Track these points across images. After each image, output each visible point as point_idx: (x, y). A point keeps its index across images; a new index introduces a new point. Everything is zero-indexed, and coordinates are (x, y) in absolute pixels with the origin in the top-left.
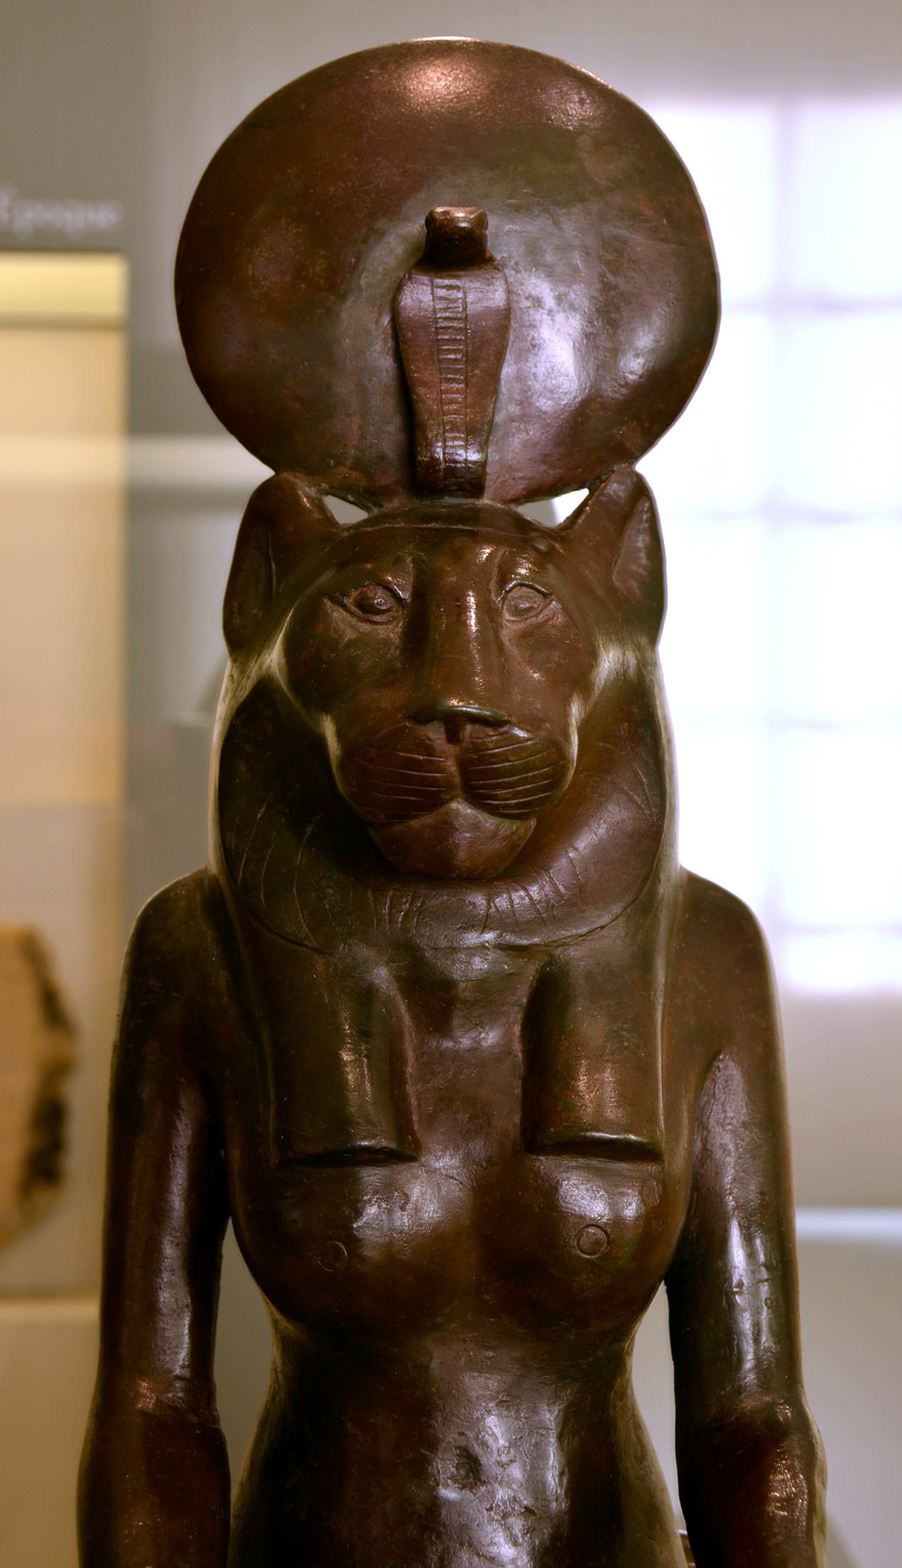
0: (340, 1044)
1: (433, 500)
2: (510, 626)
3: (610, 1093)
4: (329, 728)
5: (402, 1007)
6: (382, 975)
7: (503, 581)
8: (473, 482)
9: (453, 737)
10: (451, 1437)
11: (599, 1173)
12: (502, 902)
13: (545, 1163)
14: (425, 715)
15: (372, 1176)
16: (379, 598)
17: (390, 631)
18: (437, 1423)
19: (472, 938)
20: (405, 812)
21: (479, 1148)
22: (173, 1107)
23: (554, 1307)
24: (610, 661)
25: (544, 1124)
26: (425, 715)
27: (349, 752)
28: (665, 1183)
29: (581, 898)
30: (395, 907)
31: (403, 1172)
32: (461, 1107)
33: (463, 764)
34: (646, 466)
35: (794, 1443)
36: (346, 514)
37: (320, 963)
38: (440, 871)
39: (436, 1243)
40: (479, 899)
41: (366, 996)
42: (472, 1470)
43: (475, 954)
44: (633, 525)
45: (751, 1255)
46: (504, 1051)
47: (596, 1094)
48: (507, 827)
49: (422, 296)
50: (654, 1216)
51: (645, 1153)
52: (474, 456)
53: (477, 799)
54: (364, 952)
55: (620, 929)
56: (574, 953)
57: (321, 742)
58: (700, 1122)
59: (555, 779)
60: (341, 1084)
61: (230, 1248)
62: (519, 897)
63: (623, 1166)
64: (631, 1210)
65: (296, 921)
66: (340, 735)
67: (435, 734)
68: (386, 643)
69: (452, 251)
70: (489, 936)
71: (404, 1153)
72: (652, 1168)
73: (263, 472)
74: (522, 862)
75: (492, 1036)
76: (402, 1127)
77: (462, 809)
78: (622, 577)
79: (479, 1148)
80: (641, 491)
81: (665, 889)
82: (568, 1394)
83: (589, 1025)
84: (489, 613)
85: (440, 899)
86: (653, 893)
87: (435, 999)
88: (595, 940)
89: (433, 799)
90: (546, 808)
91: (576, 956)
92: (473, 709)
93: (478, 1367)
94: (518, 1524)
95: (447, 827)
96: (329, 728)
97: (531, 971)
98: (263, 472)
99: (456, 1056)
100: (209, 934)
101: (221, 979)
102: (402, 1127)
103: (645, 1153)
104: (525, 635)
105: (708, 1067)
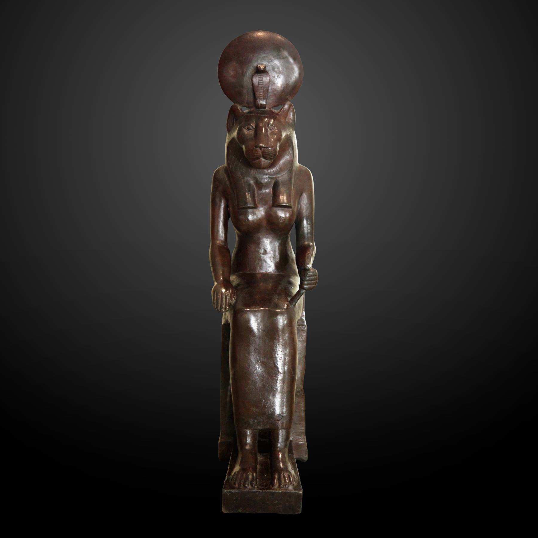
0: (246, 192)
2: (269, 131)
3: (285, 199)
4: (244, 147)
5: (255, 187)
6: (252, 182)
7: (268, 125)
8: (264, 107)
9: (261, 149)
10: (262, 247)
11: (283, 210)
12: (269, 171)
13: (275, 209)
14: (257, 147)
15: (250, 210)
16: (250, 127)
17: (252, 132)
18: (261, 245)
19: (265, 176)
20: (255, 160)
21: (266, 207)
22: (221, 201)
24: (284, 135)
25: (276, 203)
26: (257, 147)
27: (246, 151)
28: (293, 211)
29: (281, 170)
30: (253, 172)
31: (255, 210)
32: (264, 201)
33: (262, 153)
36: (246, 111)
37: (243, 181)
38: (259, 167)
39: (260, 221)
40: (266, 171)
41: (250, 185)
42: (265, 252)
43: (265, 179)
46: (270, 193)
47: (283, 199)
48: (269, 161)
49: (256, 80)
50: (291, 216)
51: (289, 207)
52: (264, 103)
53: (264, 158)
54: (249, 179)
55: (287, 175)
56: (280, 178)
57: (242, 149)
58: (299, 203)
59: (275, 155)
60: (246, 198)
62: (272, 170)
63: (286, 209)
64: (288, 215)
65: (239, 174)
66: (246, 148)
67: (258, 149)
68: (251, 134)
69: (259, 71)
70: (267, 176)
71: (255, 207)
72: (291, 209)
73: (233, 104)
74: (272, 166)
75: (268, 191)
76: (255, 203)
77: (262, 159)
79: (266, 207)
81: (294, 169)
82: (280, 241)
83: (282, 189)
84: (266, 130)
85: (260, 170)
86: (292, 169)
87: (260, 185)
88: (283, 177)
89: (258, 158)
91: (280, 179)
92: (263, 146)
93: (266, 238)
94: (272, 259)
95: (260, 162)
96: (244, 147)
97: (273, 181)
99: (263, 193)
100: (226, 176)
101: (228, 183)
102: (255, 203)
103: (289, 207)
104: (271, 133)
105: (301, 195)
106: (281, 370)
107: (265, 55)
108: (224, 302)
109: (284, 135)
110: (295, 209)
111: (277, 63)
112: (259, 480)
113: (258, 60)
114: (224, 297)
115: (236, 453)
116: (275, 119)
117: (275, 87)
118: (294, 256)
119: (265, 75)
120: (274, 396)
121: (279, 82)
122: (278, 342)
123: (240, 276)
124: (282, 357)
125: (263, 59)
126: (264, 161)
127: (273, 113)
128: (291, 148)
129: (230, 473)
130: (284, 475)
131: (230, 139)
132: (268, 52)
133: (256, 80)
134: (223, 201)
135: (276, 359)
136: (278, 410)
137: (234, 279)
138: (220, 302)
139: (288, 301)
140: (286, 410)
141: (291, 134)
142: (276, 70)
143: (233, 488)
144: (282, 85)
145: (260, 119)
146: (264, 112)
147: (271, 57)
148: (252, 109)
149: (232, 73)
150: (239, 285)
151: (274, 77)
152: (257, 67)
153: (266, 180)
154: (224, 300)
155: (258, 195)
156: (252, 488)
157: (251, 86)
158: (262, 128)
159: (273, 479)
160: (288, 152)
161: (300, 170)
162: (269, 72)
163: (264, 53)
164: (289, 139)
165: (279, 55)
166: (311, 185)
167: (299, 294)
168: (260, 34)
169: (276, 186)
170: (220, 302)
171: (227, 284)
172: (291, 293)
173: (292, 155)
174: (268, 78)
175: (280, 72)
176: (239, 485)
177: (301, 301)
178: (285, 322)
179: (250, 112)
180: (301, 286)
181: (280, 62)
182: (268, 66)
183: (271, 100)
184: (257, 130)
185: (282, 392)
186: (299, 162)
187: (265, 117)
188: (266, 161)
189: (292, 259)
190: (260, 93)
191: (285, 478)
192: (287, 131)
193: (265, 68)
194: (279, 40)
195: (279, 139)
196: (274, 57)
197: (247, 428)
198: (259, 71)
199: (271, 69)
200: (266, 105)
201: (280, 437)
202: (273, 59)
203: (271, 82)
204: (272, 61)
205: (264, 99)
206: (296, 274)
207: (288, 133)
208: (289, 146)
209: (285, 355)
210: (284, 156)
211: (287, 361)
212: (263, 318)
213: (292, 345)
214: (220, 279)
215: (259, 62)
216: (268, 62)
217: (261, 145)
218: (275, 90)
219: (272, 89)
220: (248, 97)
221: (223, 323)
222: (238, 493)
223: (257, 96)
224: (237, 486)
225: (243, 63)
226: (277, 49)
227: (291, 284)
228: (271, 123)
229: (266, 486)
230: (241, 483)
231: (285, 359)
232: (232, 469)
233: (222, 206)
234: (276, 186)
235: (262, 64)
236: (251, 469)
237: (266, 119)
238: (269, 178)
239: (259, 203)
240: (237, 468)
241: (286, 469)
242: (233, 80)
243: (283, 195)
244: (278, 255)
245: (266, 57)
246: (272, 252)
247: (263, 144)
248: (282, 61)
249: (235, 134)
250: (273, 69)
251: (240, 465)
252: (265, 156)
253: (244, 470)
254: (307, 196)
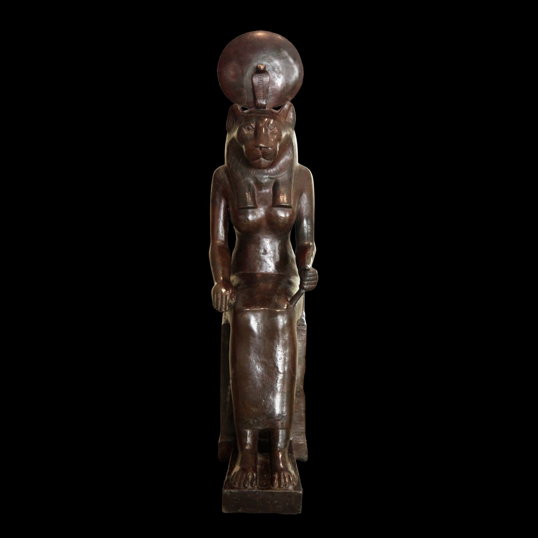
0: (246, 192)
2: (269, 131)
3: (285, 199)
4: (244, 147)
5: (255, 187)
6: (252, 182)
7: (268, 125)
8: (264, 107)
9: (261, 149)
10: (262, 247)
11: (283, 210)
12: (269, 171)
13: (275, 209)
14: (257, 147)
15: (250, 210)
16: (250, 127)
17: (252, 132)
18: (261, 245)
19: (265, 176)
20: (255, 160)
21: (266, 207)
22: (221, 201)
24: (284, 135)
25: (276, 203)
26: (257, 147)
27: (246, 151)
28: (293, 211)
29: (281, 170)
30: (253, 172)
31: (255, 210)
32: (264, 201)
33: (262, 153)
37: (243, 181)
38: (259, 167)
39: (260, 221)
40: (266, 171)
41: (250, 185)
42: (265, 252)
43: (265, 179)
45: (307, 223)
46: (270, 193)
47: (283, 199)
48: (269, 161)
49: (256, 80)
50: (291, 216)
51: (289, 207)
52: (264, 103)
53: (264, 158)
54: (249, 179)
55: (287, 175)
56: (280, 178)
57: (242, 149)
58: (299, 203)
59: (275, 155)
60: (246, 198)
62: (272, 170)
63: (286, 209)
64: (288, 215)
65: (239, 174)
66: (246, 148)
67: (258, 149)
68: (251, 134)
69: (259, 71)
70: (267, 176)
71: (255, 207)
72: (291, 209)
74: (272, 166)
75: (268, 191)
76: (255, 203)
77: (262, 159)
79: (266, 207)
82: (280, 241)
83: (282, 189)
84: (266, 130)
85: (260, 170)
86: (292, 169)
87: (260, 185)
88: (283, 177)
89: (258, 158)
91: (280, 179)
92: (263, 146)
93: (266, 238)
94: (272, 259)
95: (260, 162)
96: (244, 147)
97: (273, 181)
99: (263, 193)
100: (226, 176)
101: (228, 183)
102: (255, 203)
103: (289, 207)
104: (271, 133)
105: (301, 195)
106: (281, 370)
107: (265, 55)
108: (224, 302)
109: (284, 135)
110: (295, 209)
111: (277, 63)
112: (259, 480)
113: (258, 60)
114: (224, 297)
115: (236, 453)
116: (275, 119)
117: (275, 87)
118: (294, 256)
119: (265, 75)
120: (274, 396)
121: (279, 82)
122: (278, 342)
123: (240, 276)
124: (282, 357)
125: (263, 59)
126: (264, 161)
127: (273, 113)
128: (291, 148)
129: (230, 473)
130: (284, 475)
131: (230, 139)
132: (268, 52)
133: (256, 80)
134: (223, 201)
135: (276, 359)
136: (278, 410)
137: (234, 279)
138: (220, 302)
139: (288, 301)
141: (291, 134)
142: (276, 70)
143: (233, 488)
144: (282, 85)
145: (260, 119)
146: (264, 112)
147: (271, 57)
148: (252, 109)
149: (232, 73)
150: (239, 285)
151: (274, 77)
152: (257, 67)
153: (266, 180)
154: (224, 300)
155: (258, 195)
156: (252, 488)
157: (251, 86)
158: (262, 128)
159: (273, 479)
160: (288, 152)
161: (300, 170)
162: (269, 72)
163: (264, 53)
164: (289, 139)
165: (279, 55)
166: (311, 185)
167: (299, 293)
168: (260, 34)
169: (276, 186)
170: (220, 302)
171: (227, 284)
172: (291, 293)
173: (292, 155)
174: (268, 78)
175: (280, 72)
176: (239, 485)
177: (301, 301)
178: (285, 322)
179: (250, 112)
180: (301, 286)
181: (280, 62)
182: (268, 66)
184: (257, 130)
185: (282, 392)
186: (299, 162)
187: (265, 117)
188: (266, 161)
189: (292, 259)
190: (260, 93)
191: (285, 478)
192: (287, 131)
193: (265, 68)
194: (279, 40)
195: (279, 139)
196: (274, 57)
197: (247, 428)
198: (259, 71)
199: (271, 69)
200: (266, 105)
201: (280, 437)
202: (273, 59)
203: (271, 82)
204: (272, 61)
205: (264, 99)
206: (296, 274)
207: (288, 133)
208: (289, 146)
209: (285, 355)
210: (284, 156)
211: (287, 361)
212: (263, 318)
213: (292, 345)
214: (220, 279)
215: (259, 62)
216: (268, 62)
217: (261, 145)
218: (275, 90)
219: (272, 89)
220: (248, 97)
221: (223, 323)
222: (238, 493)
223: (257, 96)
224: (237, 486)
226: (277, 49)
227: (291, 284)
228: (271, 123)
229: (266, 486)
230: (241, 483)
231: (285, 359)
232: (232, 469)
233: (222, 206)
234: (276, 186)
235: (262, 64)
236: (251, 469)
237: (266, 119)
238: (269, 178)
239: (259, 203)
240: (237, 468)
241: (286, 469)
242: (233, 80)
243: (283, 195)
244: (278, 255)
245: (266, 57)
246: (272, 252)
247: (263, 144)
248: (282, 61)
249: (235, 134)
250: (273, 69)
251: (240, 465)
252: (265, 156)
253: (244, 470)
254: (307, 196)
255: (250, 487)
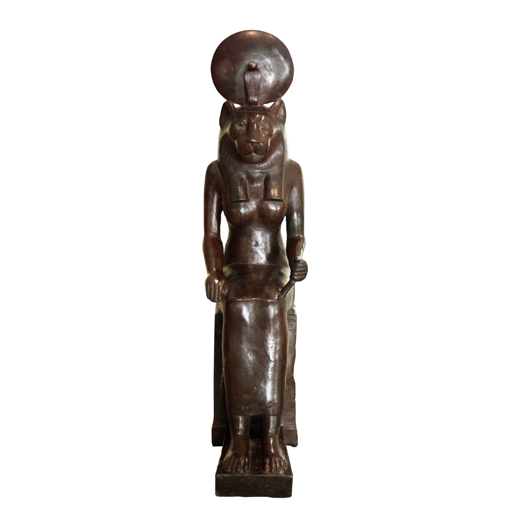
0: (238, 186)
1: (251, 109)
2: (261, 127)
3: (276, 193)
4: (236, 142)
5: (247, 181)
6: (244, 176)
7: (260, 121)
8: (256, 103)
9: (252, 145)
10: (254, 240)
11: (274, 203)
12: (261, 166)
13: (266, 202)
14: (249, 142)
15: (242, 204)
16: (242, 123)
17: (244, 128)
18: (252, 237)
19: (256, 171)
20: (246, 155)
21: (258, 200)
22: (214, 195)
23: (271, 224)
24: (275, 130)
25: (267, 197)
26: (249, 142)
27: (239, 146)
28: (284, 204)
29: (272, 165)
30: (245, 167)
31: (247, 203)
32: (255, 195)
33: (254, 148)
34: (283, 98)
35: (302, 240)
37: (235, 175)
38: (251, 162)
39: (252, 214)
40: (258, 165)
41: (242, 179)
42: (257, 244)
43: (257, 173)
44: (281, 107)
45: (297, 216)
46: (261, 186)
47: (274, 192)
48: (260, 156)
49: (248, 77)
50: (282, 209)
51: (280, 200)
52: (256, 100)
53: (256, 153)
54: (241, 173)
55: (277, 169)
56: (271, 173)
57: (235, 144)
58: (290, 197)
59: (266, 150)
60: (238, 192)
61: (223, 214)
62: (263, 165)
63: (277, 202)
64: (279, 208)
65: (231, 169)
66: (238, 143)
67: (250, 144)
68: (243, 130)
70: (259, 171)
71: (247, 201)
72: (281, 203)
73: (225, 100)
74: (263, 160)
75: (259, 185)
76: (247, 197)
77: (254, 154)
78: (278, 116)
79: (258, 200)
80: (282, 102)
81: (285, 163)
82: (271, 234)
83: (273, 183)
84: (258, 126)
85: (252, 165)
86: (283, 164)
87: (252, 179)
88: (274, 171)
89: (250, 153)
90: (266, 153)
91: (271, 173)
92: (255, 141)
93: (258, 230)
94: (263, 251)
95: (252, 157)
96: (236, 142)
97: (265, 175)
98: (225, 100)
99: (254, 187)
100: (219, 170)
101: (221, 177)
102: (247, 197)
103: (280, 200)
104: (263, 129)
105: (291, 188)
106: (272, 358)
107: (257, 53)
108: (217, 293)
109: (275, 130)
110: (286, 203)
111: (268, 61)
112: (251, 465)
113: (249, 58)
114: (217, 287)
116: (266, 115)
117: (266, 85)
119: (256, 73)
120: (265, 383)
122: (270, 331)
123: (232, 267)
124: (274, 345)
125: (255, 57)
126: (256, 156)
128: (282, 144)
130: (275, 460)
132: (260, 50)
133: (248, 77)
134: (216, 195)
135: (268, 348)
136: (269, 397)
137: (226, 270)
138: (213, 292)
139: (279, 291)
140: (277, 397)
142: (267, 67)
143: (226, 473)
144: (273, 82)
145: (251, 115)
146: (256, 109)
147: (262, 55)
148: (245, 106)
149: (225, 71)
150: (231, 276)
151: (266, 75)
152: (249, 65)
153: (257, 175)
154: (217, 290)
155: (250, 189)
157: (243, 84)
158: (254, 124)
159: (264, 464)
160: (278, 148)
162: (261, 70)
163: (256, 52)
165: (270, 53)
169: (267, 180)
170: (213, 292)
172: (281, 283)
173: (283, 150)
174: (260, 76)
175: (271, 70)
176: (232, 470)
178: (276, 312)
181: (271, 60)
182: (259, 64)
183: (263, 96)
184: (249, 126)
185: (273, 380)
187: (257, 114)
188: (258, 156)
189: (283, 251)
190: (252, 90)
191: (276, 463)
192: (277, 127)
193: (257, 65)
195: (270, 135)
196: (265, 55)
197: (239, 415)
198: (251, 69)
199: (263, 67)
200: (257, 101)
201: (271, 423)
202: (264, 57)
203: (263, 80)
204: (263, 59)
205: (255, 96)
206: (286, 266)
207: (279, 129)
208: (280, 141)
209: (276, 344)
210: (275, 151)
211: (278, 349)
214: (213, 270)
215: (251, 60)
216: (260, 60)
217: (253, 140)
218: (266, 87)
219: (263, 86)
222: (230, 477)
223: (249, 93)
224: (229, 470)
225: (236, 61)
227: (281, 275)
228: (263, 119)
229: (257, 470)
231: (276, 348)
233: (215, 200)
234: (267, 180)
235: (254, 62)
236: (243, 454)
237: (258, 116)
238: (260, 172)
239: (251, 197)
243: (274, 189)
244: (269, 247)
245: (258, 55)
246: (263, 244)
247: (255, 139)
248: (273, 59)
250: (265, 67)
251: (233, 450)
252: (256, 151)
254: (297, 190)
255: (242, 471)
